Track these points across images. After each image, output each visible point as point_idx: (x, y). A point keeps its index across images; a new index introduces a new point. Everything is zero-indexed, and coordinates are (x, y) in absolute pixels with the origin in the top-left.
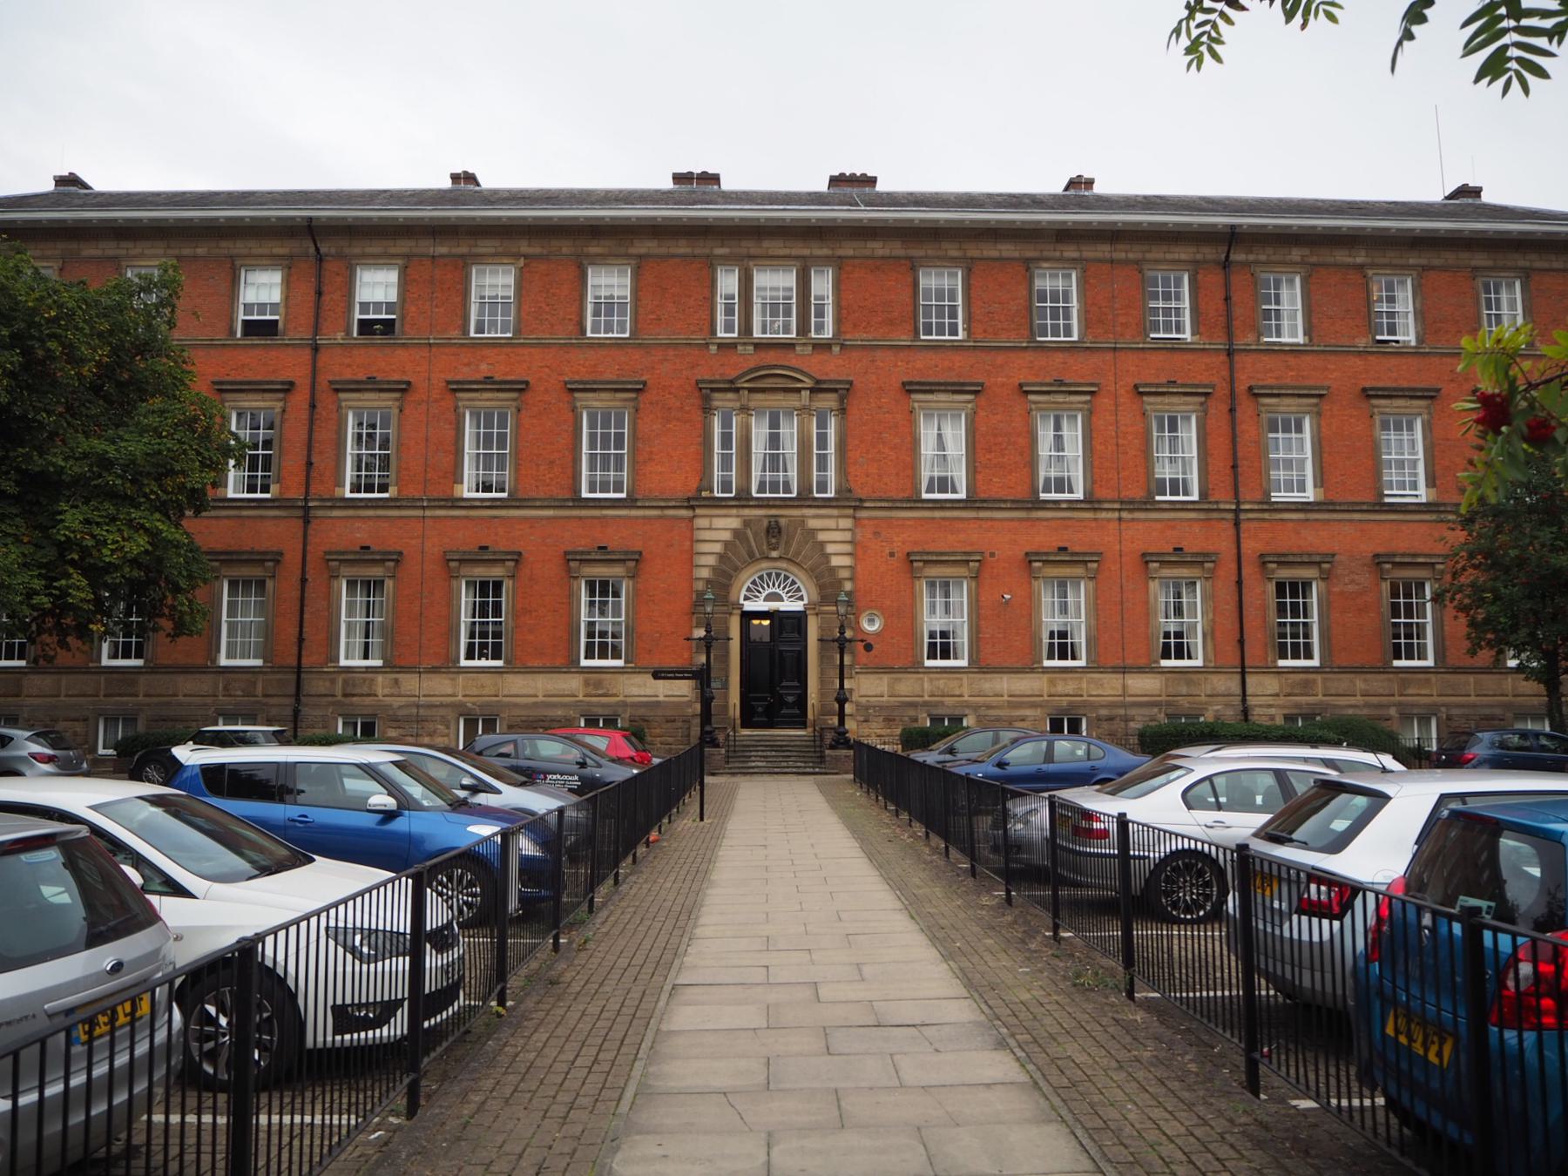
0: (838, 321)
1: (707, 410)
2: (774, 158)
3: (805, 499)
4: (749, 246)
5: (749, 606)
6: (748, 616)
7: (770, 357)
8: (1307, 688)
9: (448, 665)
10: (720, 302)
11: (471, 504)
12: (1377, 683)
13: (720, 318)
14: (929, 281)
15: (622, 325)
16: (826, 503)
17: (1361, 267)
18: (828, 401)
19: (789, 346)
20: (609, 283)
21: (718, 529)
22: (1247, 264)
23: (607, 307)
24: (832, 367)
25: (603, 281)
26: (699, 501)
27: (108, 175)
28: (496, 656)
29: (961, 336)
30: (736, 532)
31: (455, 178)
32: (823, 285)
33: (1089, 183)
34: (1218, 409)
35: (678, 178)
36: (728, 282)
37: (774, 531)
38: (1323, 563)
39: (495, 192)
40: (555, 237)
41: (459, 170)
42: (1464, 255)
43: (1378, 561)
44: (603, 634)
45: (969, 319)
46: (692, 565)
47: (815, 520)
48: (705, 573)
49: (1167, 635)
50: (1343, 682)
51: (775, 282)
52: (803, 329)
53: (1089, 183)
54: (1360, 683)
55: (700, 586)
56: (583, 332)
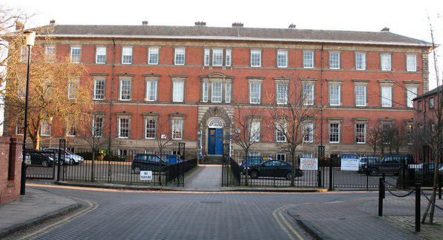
0: (232, 62)
1: (201, 82)
2: (219, 19)
3: (223, 102)
4: (212, 44)
5: (210, 127)
6: (210, 129)
7: (216, 70)
8: (336, 148)
9: (143, 138)
10: (205, 57)
11: (148, 102)
12: (352, 147)
13: (205, 61)
14: (253, 52)
15: (220, 63)
16: (228, 104)
17: (353, 52)
18: (229, 80)
19: (221, 68)
20: (180, 52)
21: (203, 109)
22: (327, 50)
23: (179, 57)
24: (230, 73)
25: (152, 50)
26: (199, 102)
27: (153, 22)
28: (127, 136)
29: (260, 66)
30: (208, 110)
31: (143, 23)
32: (229, 53)
33: (295, 26)
34: (318, 83)
35: (196, 23)
36: (207, 52)
37: (216, 109)
38: (341, 119)
39: (252, 29)
40: (168, 38)
41: (197, 21)
42: (378, 49)
43: (353, 120)
44: (334, 136)
45: (262, 62)
46: (198, 115)
47: (225, 107)
48: (200, 119)
49: (331, 136)
50: (344, 146)
51: (218, 52)
52: (224, 64)
53: (295, 26)
54: (348, 147)
55: (199, 122)
56: (95, 62)
